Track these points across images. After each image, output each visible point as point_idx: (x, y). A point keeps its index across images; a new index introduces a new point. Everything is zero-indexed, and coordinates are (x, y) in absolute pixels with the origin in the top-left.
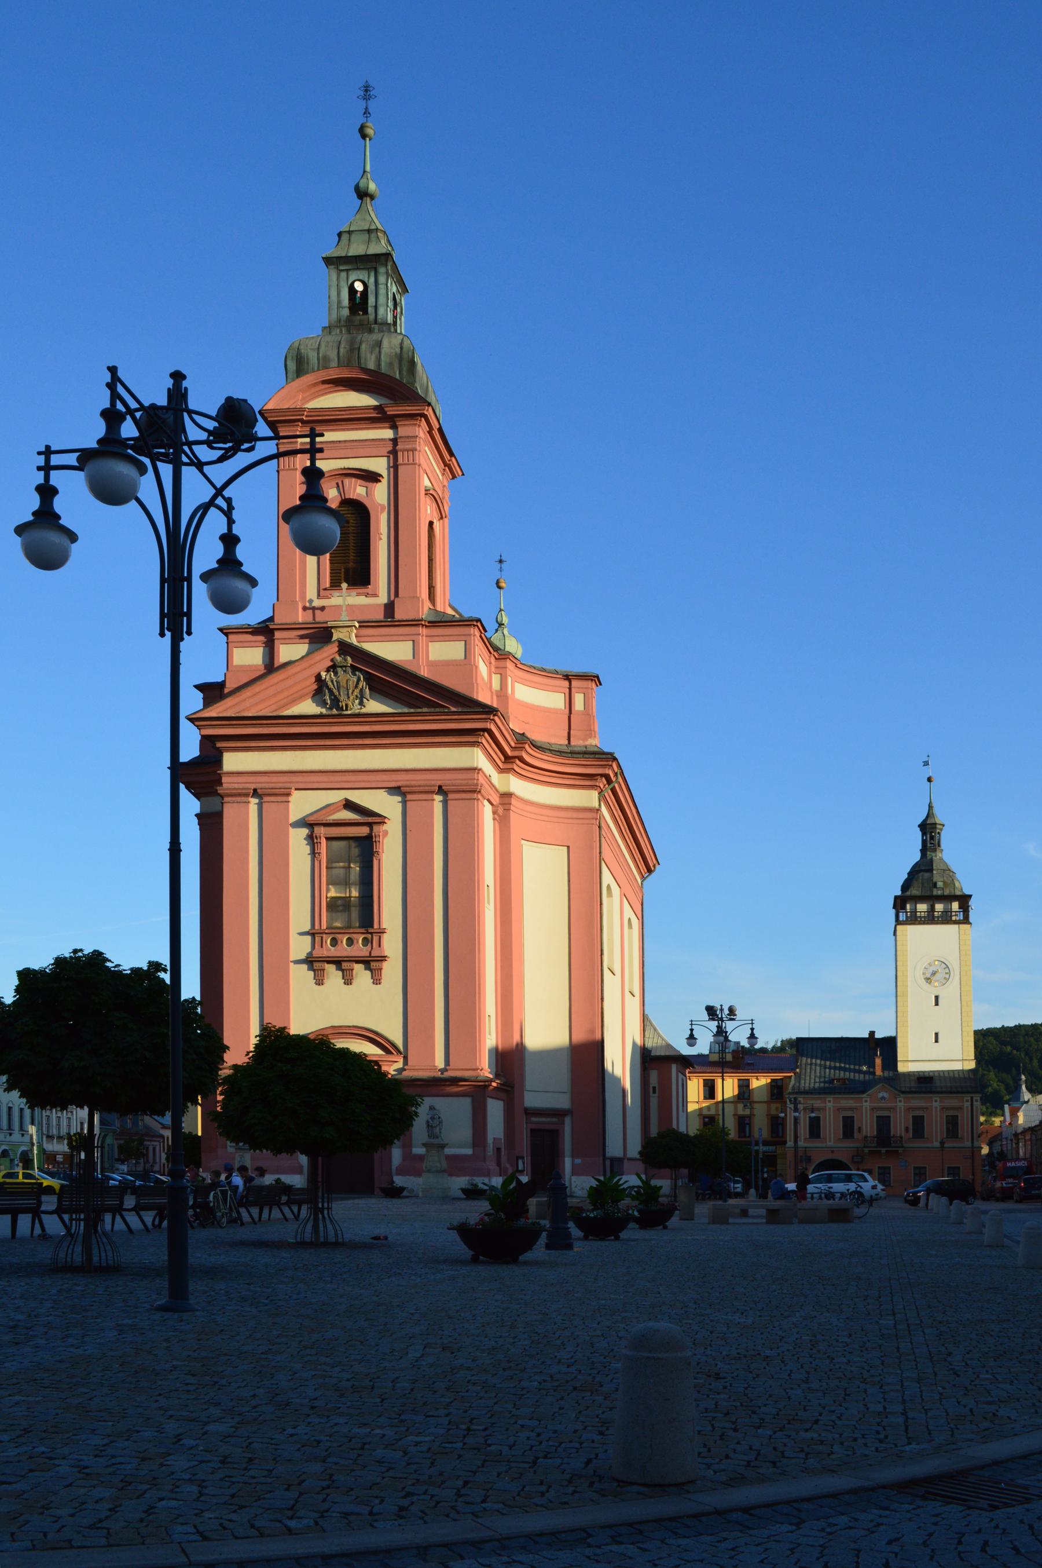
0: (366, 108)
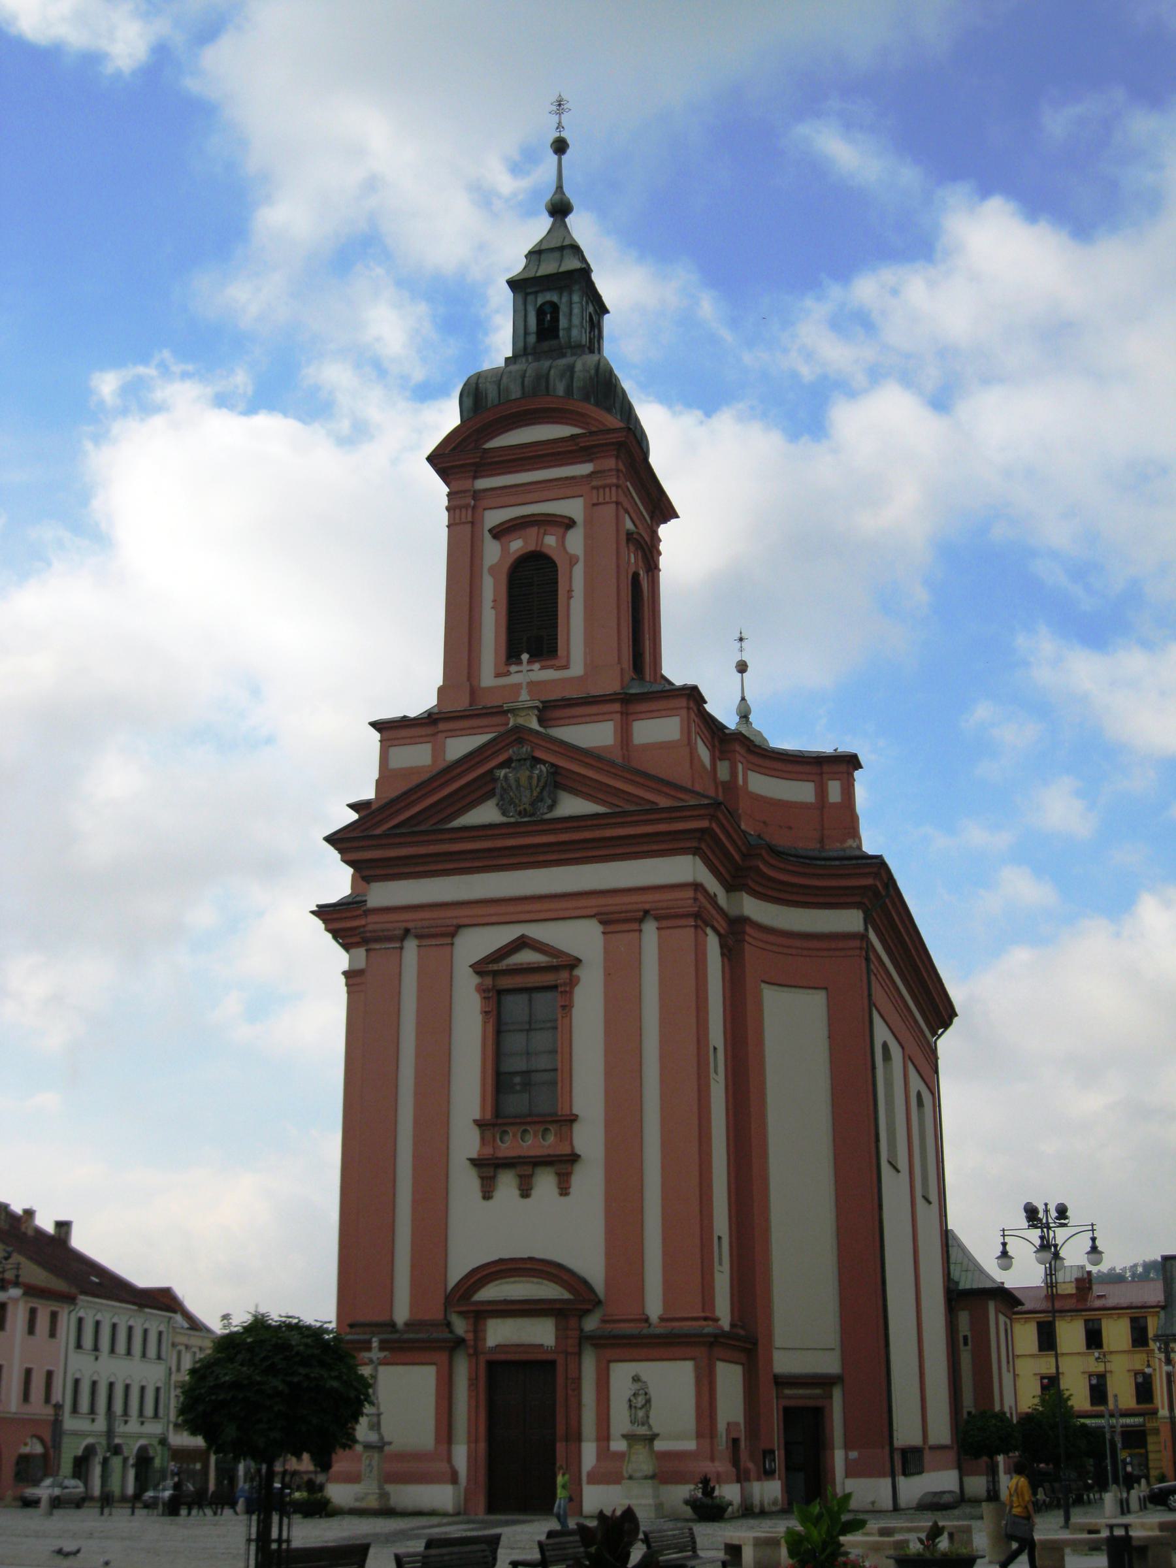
0: (560, 123)
